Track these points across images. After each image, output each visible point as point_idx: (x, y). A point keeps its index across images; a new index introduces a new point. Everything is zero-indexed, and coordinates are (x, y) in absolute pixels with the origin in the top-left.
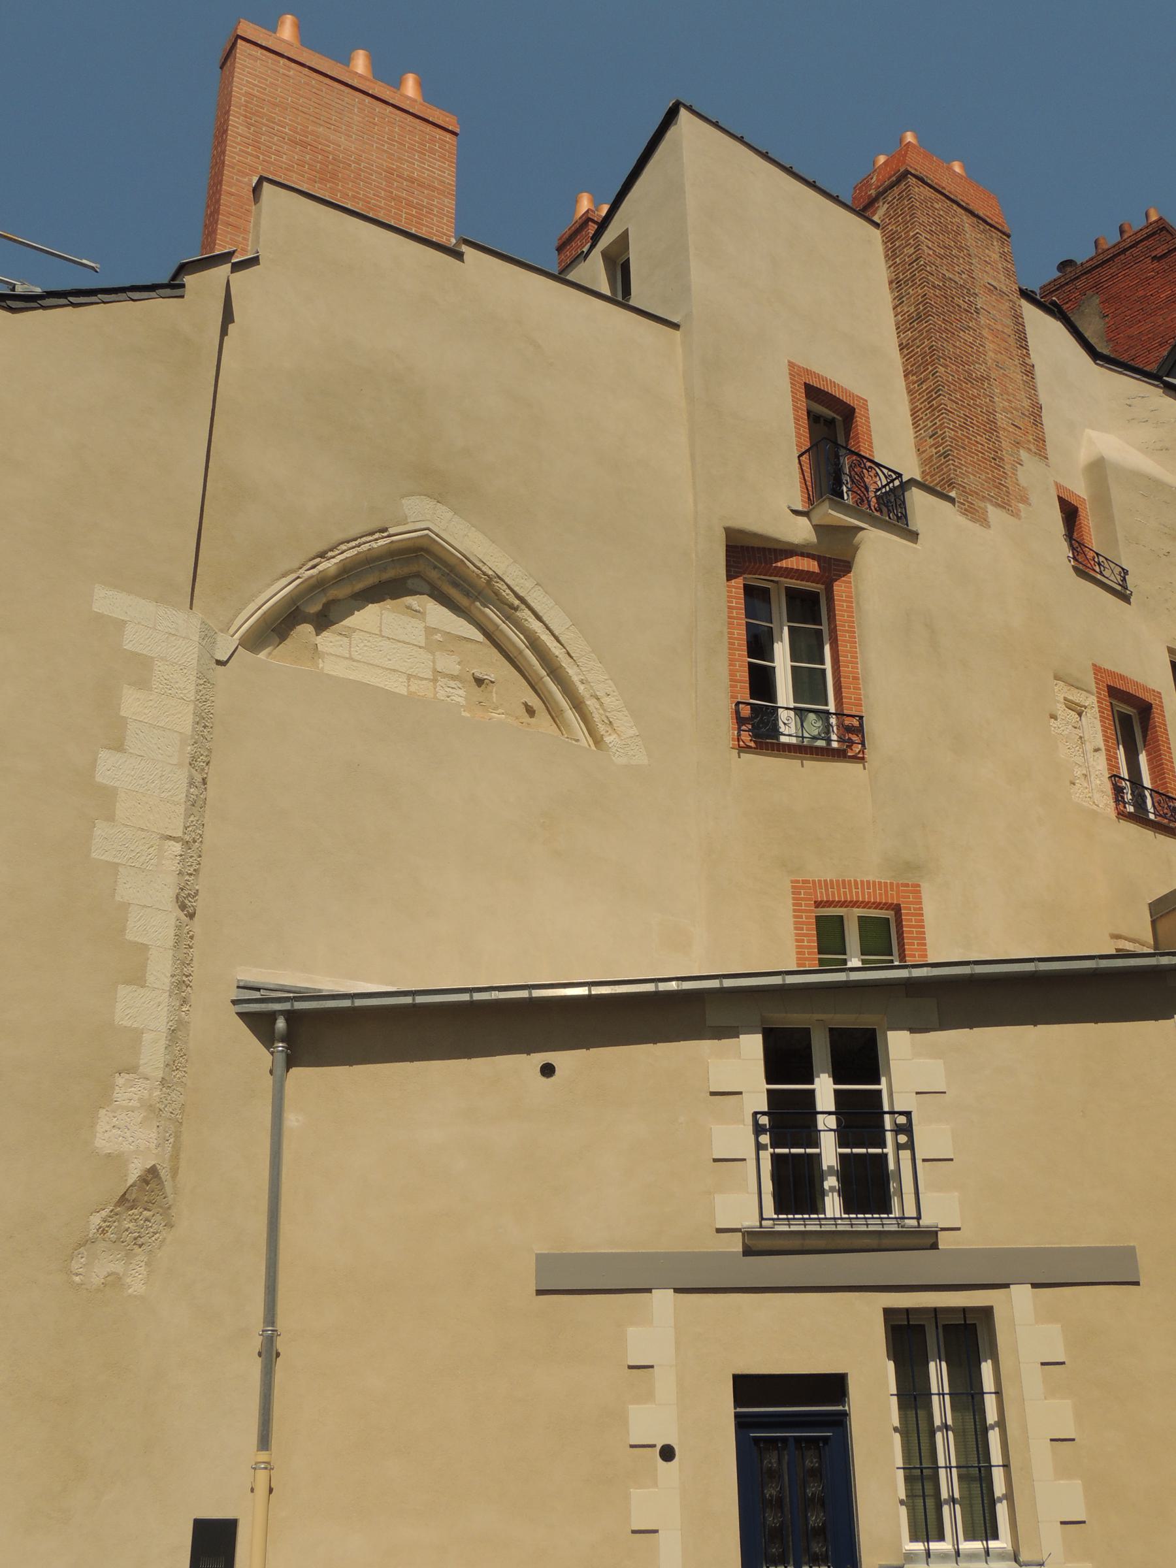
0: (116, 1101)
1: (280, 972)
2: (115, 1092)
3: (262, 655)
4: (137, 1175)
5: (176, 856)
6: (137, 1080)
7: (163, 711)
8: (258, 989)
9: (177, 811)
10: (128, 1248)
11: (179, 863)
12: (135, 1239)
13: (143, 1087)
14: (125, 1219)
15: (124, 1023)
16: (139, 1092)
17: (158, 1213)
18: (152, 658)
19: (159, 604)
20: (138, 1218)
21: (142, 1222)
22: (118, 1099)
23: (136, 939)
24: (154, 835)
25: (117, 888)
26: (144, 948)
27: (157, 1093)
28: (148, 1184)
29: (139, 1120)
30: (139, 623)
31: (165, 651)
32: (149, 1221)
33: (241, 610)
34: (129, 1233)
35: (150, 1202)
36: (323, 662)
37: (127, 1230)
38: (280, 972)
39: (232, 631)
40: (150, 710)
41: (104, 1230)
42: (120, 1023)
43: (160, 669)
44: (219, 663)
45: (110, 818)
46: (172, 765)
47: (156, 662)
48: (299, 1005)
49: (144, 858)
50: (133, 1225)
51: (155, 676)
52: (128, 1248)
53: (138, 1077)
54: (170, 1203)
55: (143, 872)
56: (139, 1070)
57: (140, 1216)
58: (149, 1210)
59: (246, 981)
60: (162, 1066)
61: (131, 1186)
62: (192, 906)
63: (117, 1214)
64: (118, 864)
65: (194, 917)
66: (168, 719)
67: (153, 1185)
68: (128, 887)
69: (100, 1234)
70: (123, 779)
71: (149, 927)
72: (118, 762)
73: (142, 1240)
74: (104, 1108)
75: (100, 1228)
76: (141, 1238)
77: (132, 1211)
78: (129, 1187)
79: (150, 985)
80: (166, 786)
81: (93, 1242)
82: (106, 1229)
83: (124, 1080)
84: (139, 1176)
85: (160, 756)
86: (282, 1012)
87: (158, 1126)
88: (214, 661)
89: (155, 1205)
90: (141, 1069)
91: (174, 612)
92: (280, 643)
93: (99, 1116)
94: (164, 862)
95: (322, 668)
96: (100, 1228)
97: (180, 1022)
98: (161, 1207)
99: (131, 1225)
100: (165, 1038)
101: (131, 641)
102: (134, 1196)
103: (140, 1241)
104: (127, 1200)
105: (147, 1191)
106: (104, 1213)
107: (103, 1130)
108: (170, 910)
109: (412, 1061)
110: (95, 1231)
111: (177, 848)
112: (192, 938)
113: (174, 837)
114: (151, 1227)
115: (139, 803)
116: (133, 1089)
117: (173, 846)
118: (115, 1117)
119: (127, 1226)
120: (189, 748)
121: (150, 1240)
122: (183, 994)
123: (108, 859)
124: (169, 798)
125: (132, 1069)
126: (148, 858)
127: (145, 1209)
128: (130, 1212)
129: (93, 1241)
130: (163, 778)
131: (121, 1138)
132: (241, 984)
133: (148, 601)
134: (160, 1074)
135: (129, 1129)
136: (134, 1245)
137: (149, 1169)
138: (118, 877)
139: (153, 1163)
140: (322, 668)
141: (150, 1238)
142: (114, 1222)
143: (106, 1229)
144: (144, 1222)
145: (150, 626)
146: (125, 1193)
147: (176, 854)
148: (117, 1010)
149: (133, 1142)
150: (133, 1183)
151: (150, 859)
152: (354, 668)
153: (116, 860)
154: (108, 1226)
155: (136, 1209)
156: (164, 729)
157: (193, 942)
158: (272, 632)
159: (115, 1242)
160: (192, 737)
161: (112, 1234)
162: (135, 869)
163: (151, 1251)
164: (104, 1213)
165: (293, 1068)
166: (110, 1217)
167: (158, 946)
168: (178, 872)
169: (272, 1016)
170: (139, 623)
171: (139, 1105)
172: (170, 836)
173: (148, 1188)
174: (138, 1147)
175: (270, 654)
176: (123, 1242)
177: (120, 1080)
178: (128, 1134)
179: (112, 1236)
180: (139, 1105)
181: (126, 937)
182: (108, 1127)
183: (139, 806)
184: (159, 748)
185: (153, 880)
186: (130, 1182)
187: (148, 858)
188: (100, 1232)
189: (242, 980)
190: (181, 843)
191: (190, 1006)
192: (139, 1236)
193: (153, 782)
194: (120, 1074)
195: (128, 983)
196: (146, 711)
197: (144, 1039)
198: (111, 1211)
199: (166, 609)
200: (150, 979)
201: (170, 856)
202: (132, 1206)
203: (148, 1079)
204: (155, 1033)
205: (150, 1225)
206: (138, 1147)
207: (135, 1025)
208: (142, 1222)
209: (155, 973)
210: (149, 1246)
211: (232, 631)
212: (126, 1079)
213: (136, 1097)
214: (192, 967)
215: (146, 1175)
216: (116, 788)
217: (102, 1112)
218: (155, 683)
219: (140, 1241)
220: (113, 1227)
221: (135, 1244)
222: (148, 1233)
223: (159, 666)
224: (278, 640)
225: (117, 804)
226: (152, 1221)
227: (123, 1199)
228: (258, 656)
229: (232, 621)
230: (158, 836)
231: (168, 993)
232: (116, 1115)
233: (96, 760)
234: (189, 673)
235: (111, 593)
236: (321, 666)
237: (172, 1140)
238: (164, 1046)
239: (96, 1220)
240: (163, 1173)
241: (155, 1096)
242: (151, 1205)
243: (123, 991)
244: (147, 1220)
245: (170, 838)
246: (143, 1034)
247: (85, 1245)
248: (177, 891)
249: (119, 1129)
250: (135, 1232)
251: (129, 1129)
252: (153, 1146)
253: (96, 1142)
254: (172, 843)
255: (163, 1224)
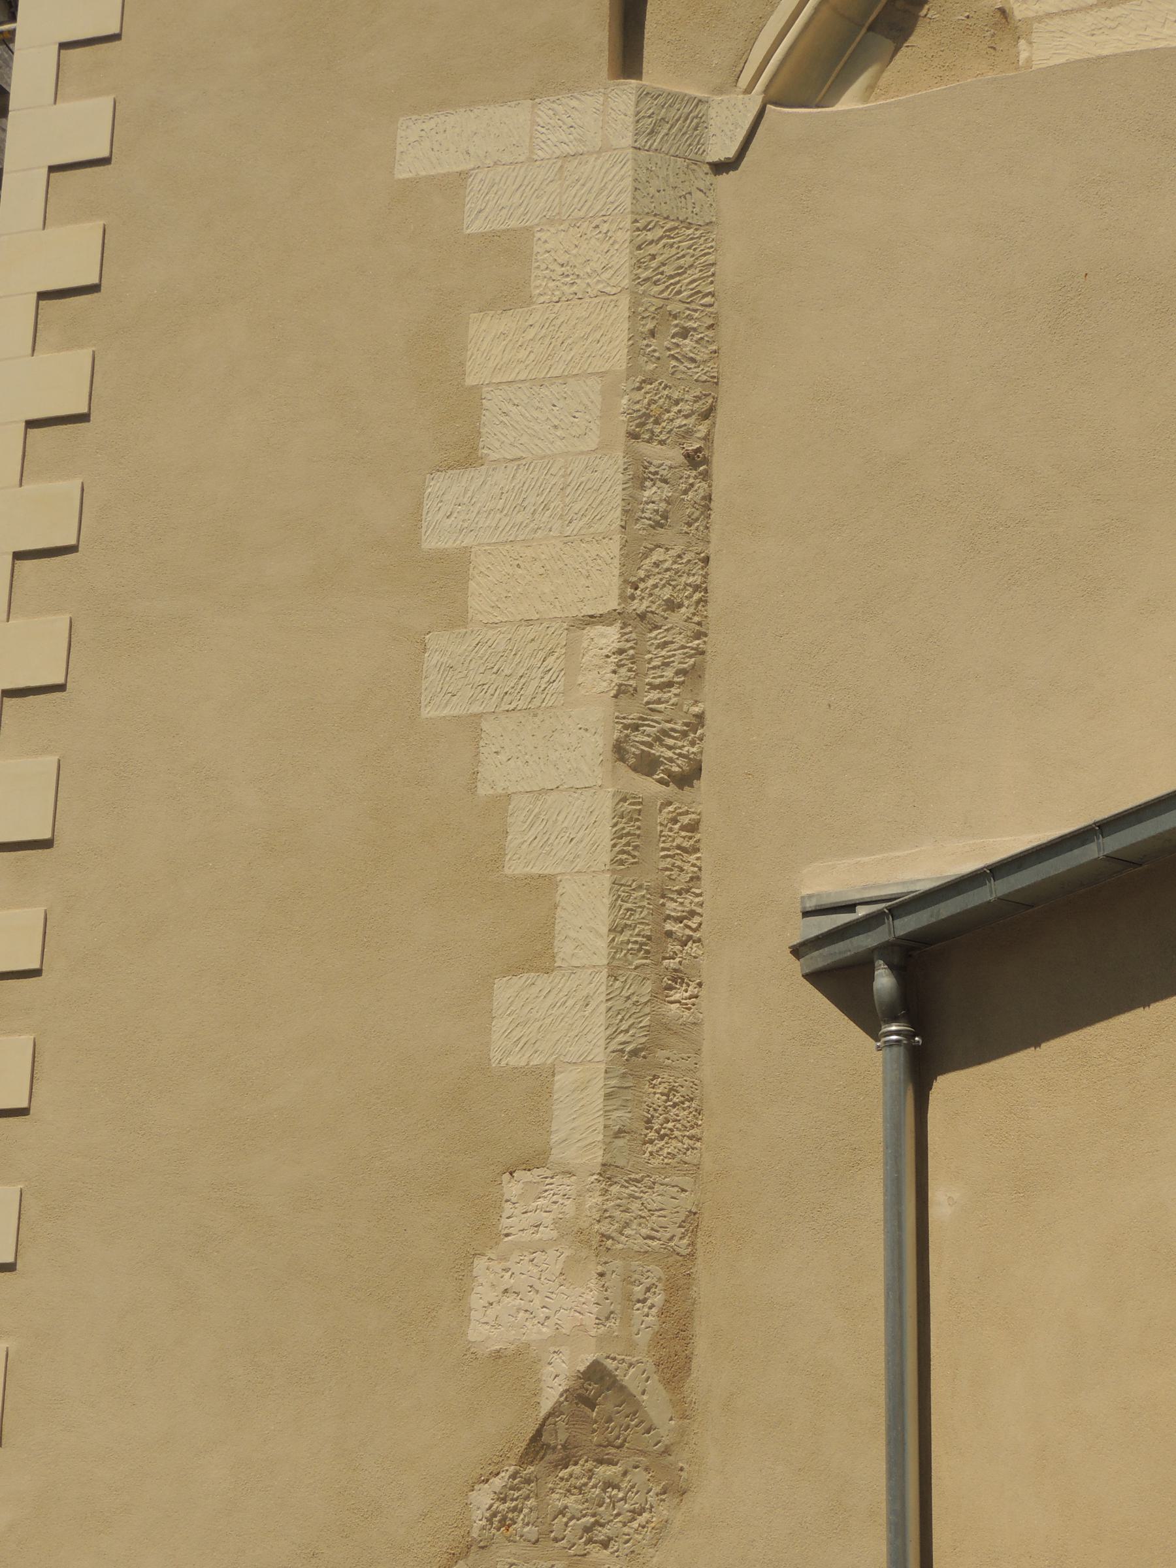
0: (507, 1235)
1: (906, 852)
2: (505, 1215)
3: (849, 102)
4: (561, 1389)
5: (608, 656)
6: (548, 1181)
7: (560, 340)
8: (850, 907)
9: (603, 554)
10: (572, 1552)
11: (614, 672)
12: (588, 1529)
13: (562, 1193)
14: (553, 1490)
15: (512, 1061)
16: (555, 1206)
17: (636, 1467)
18: (528, 229)
19: (538, 100)
20: (585, 1484)
21: (598, 1491)
22: (511, 1230)
23: (527, 870)
24: (555, 625)
25: (480, 769)
26: (549, 882)
27: (594, 1200)
28: (592, 1406)
29: (558, 1267)
30: (495, 163)
31: (557, 200)
32: (616, 1487)
33: (764, 19)
34: (571, 1519)
35: (611, 1444)
36: (1031, 43)
37: (562, 1512)
38: (906, 852)
39: (745, 81)
40: (529, 349)
41: (504, 1518)
42: (503, 1063)
43: (548, 246)
44: (720, 168)
45: (458, 620)
46: (588, 452)
47: (538, 235)
48: (907, 925)
49: (534, 684)
50: (576, 1501)
51: (538, 267)
52: (572, 1552)
53: (549, 1173)
54: (666, 1440)
55: (535, 715)
56: (552, 1158)
57: (590, 1478)
58: (611, 1463)
59: (819, 895)
60: (601, 1137)
61: (550, 1415)
62: (680, 755)
63: (528, 1481)
64: (480, 715)
65: (699, 778)
66: (572, 353)
67: (607, 1405)
68: (505, 759)
69: (498, 1530)
70: (480, 525)
71: (553, 837)
72: (466, 490)
73: (605, 1531)
74: (483, 1255)
75: (494, 1515)
76: (602, 1525)
77: (568, 1470)
78: (546, 1419)
79: (564, 965)
80: (576, 507)
81: (483, 1548)
82: (510, 1515)
83: (520, 1185)
84: (566, 1391)
85: (559, 443)
86: (884, 950)
87: (602, 1275)
88: (707, 168)
89: (624, 1449)
90: (556, 1155)
91: (574, 103)
92: (897, 50)
93: (475, 1274)
94: (580, 679)
95: (1029, 60)
96: (494, 1515)
97: (661, 1030)
98: (643, 1453)
99: (570, 1501)
100: (603, 1075)
101: (480, 212)
102: (562, 1437)
103: (601, 1533)
104: (548, 1446)
105: (596, 1422)
106: (497, 1483)
107: (483, 1302)
108: (600, 783)
109: (1145, 1004)
110: (484, 1522)
111: (609, 637)
112: (693, 827)
113: (601, 615)
114: (624, 1499)
115: (518, 566)
116: (540, 1202)
117: (603, 636)
118: (506, 1270)
119: (560, 1504)
120: (624, 401)
121: (626, 1530)
122: (672, 964)
123: (456, 712)
124: (582, 532)
125: (536, 1159)
126: (546, 680)
127: (601, 1462)
128: (564, 1473)
129: (482, 1544)
130: (569, 490)
131: (522, 1314)
132: (810, 905)
133: (513, 104)
134: (597, 1157)
135: (537, 1292)
136: (586, 1543)
137: (584, 1373)
138: (482, 743)
139: (589, 1358)
140: (1029, 60)
141: (625, 1525)
142: (527, 1498)
143: (510, 1515)
144: (604, 1491)
145: (522, 158)
146: (539, 1433)
147: (605, 652)
148: (494, 1037)
149: (547, 1318)
150: (554, 1408)
151: (550, 682)
152: (1113, 24)
153: (476, 709)
154: (514, 1509)
155: (576, 1464)
156: (563, 379)
157: (698, 836)
158: (871, 33)
159: (537, 1541)
160: (631, 371)
161: (528, 1524)
162: (518, 714)
163: (632, 1552)
164: (497, 1483)
165: (940, 1079)
166: (512, 1488)
167: (579, 872)
168: (613, 692)
169: (861, 967)
170: (495, 163)
171: (555, 1234)
172: (592, 616)
173: (594, 1414)
174: (558, 1327)
175: (871, 88)
176: (556, 1540)
177: (512, 1188)
178: (537, 1302)
179: (527, 1529)
180: (555, 1234)
181: (506, 869)
182: (492, 1296)
183: (520, 571)
184: (556, 427)
185: (559, 727)
186: (546, 1406)
187: (546, 680)
188: (496, 1524)
189: (810, 896)
190: (618, 624)
191: (700, 985)
192: (597, 1523)
193: (546, 508)
194: (511, 1174)
195: (514, 970)
196: (522, 354)
197: (556, 1086)
198: (514, 1476)
199: (555, 105)
200: (564, 950)
201: (596, 661)
202: (563, 1459)
203: (571, 1174)
204: (581, 1068)
205: (621, 1495)
206: (558, 1327)
207: (535, 1061)
208: (598, 1491)
209: (572, 934)
210: (627, 1542)
211: (745, 81)
212: (526, 1183)
213: (547, 1218)
214: (698, 895)
215: (582, 1387)
216: (467, 550)
217: (480, 1264)
218: (538, 282)
219: (601, 1533)
220: (526, 1511)
221: (590, 1541)
222: (618, 1515)
223: (546, 242)
224: (889, 44)
225: (472, 584)
226: (623, 1485)
227: (536, 1447)
228: (838, 107)
229: (743, 58)
230: (565, 625)
231: (605, 973)
232: (508, 1264)
233: (420, 505)
234: (614, 227)
235: (432, 123)
236: (1023, 56)
237: (658, 1299)
238: (602, 1093)
239: (483, 1498)
240: (630, 1379)
241: (590, 1207)
242: (613, 1451)
243: (505, 990)
244: (609, 1484)
245: (592, 620)
246: (553, 1075)
247: (466, 1556)
248: (616, 735)
249: (517, 1294)
250: (584, 1516)
251: (537, 1292)
252: (589, 1320)
253: (470, 1331)
254: (600, 629)
255: (658, 1489)
